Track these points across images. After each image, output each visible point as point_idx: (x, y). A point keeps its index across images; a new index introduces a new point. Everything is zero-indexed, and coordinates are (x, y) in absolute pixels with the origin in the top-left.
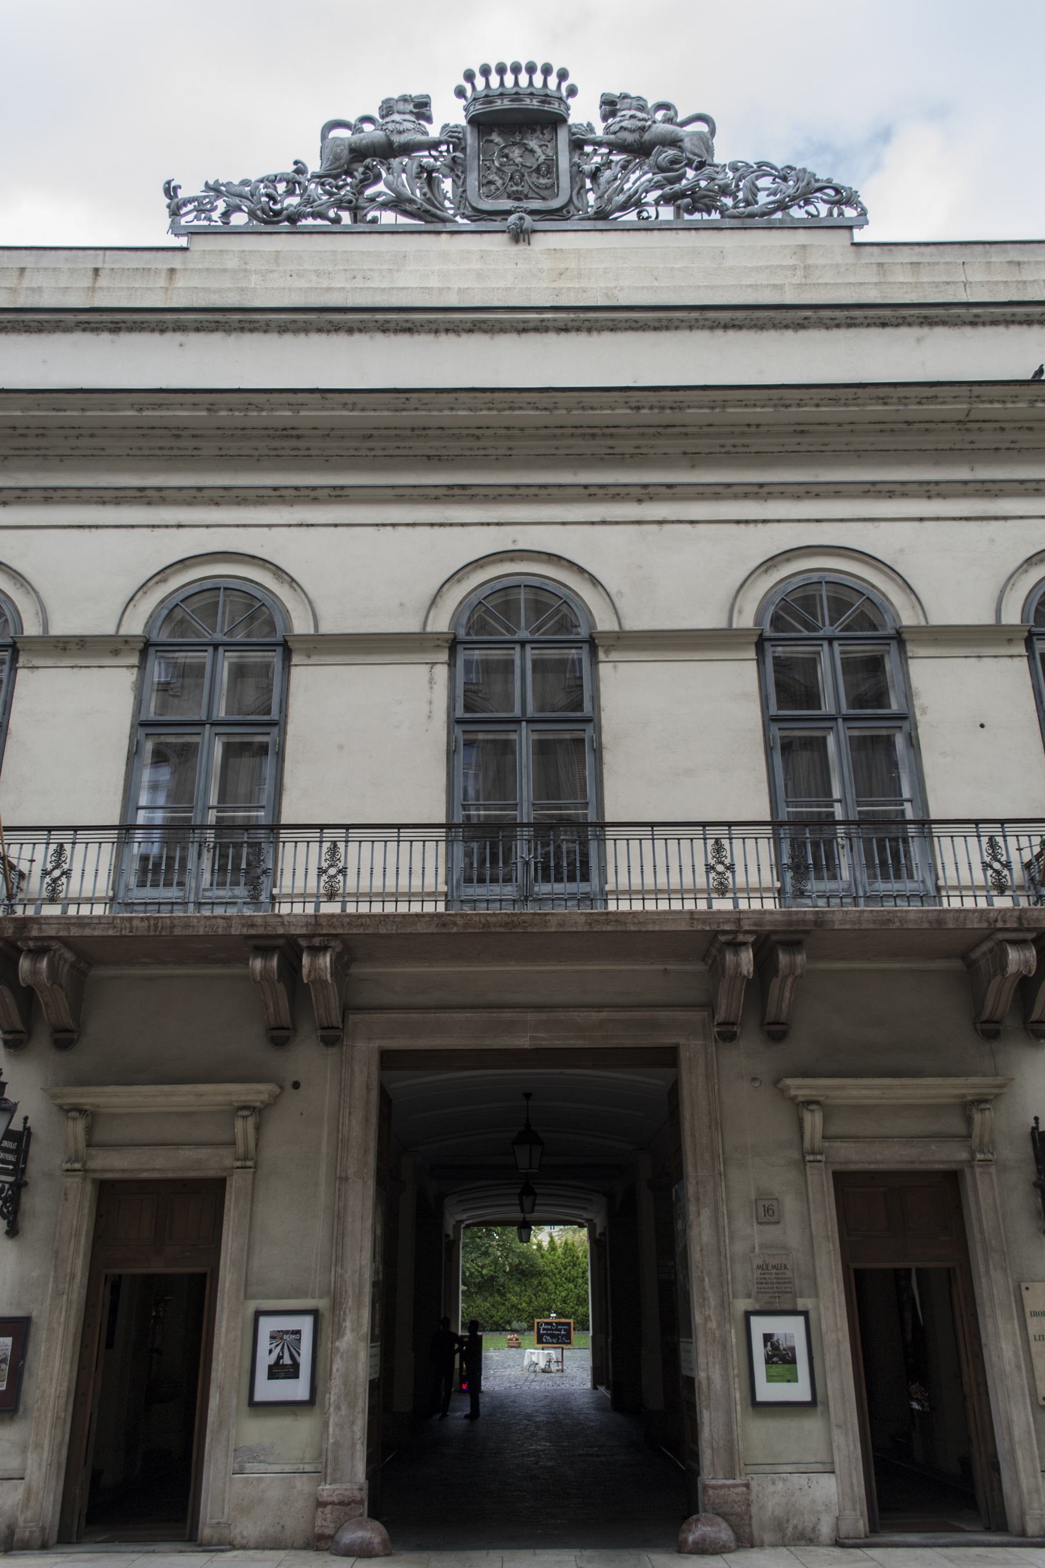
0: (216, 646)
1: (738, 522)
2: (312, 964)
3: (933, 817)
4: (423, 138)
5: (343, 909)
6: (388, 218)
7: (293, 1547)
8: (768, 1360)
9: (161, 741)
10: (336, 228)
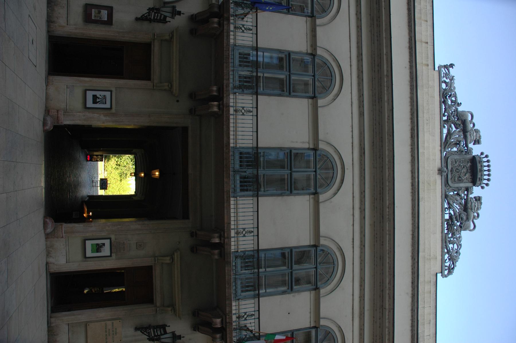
0: (314, 76)
1: (353, 239)
2: (214, 105)
3: (260, 299)
4: (469, 142)
5: (231, 115)
6: (445, 131)
7: (46, 103)
8: (97, 244)
9: (285, 59)
10: (442, 115)
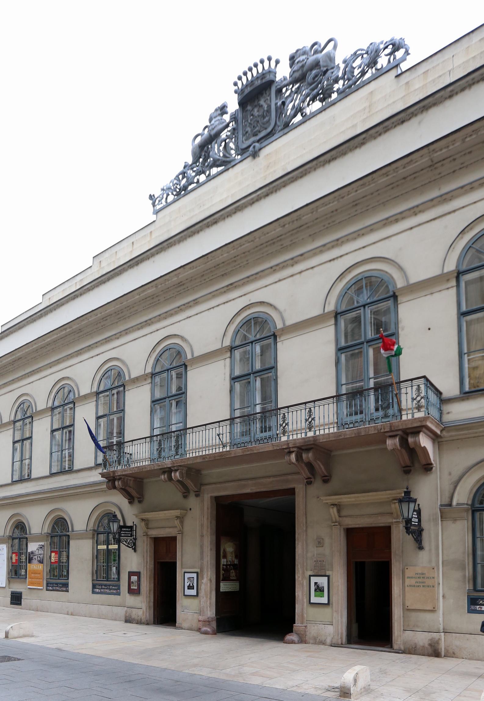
2: (175, 475)
8: (315, 590)
